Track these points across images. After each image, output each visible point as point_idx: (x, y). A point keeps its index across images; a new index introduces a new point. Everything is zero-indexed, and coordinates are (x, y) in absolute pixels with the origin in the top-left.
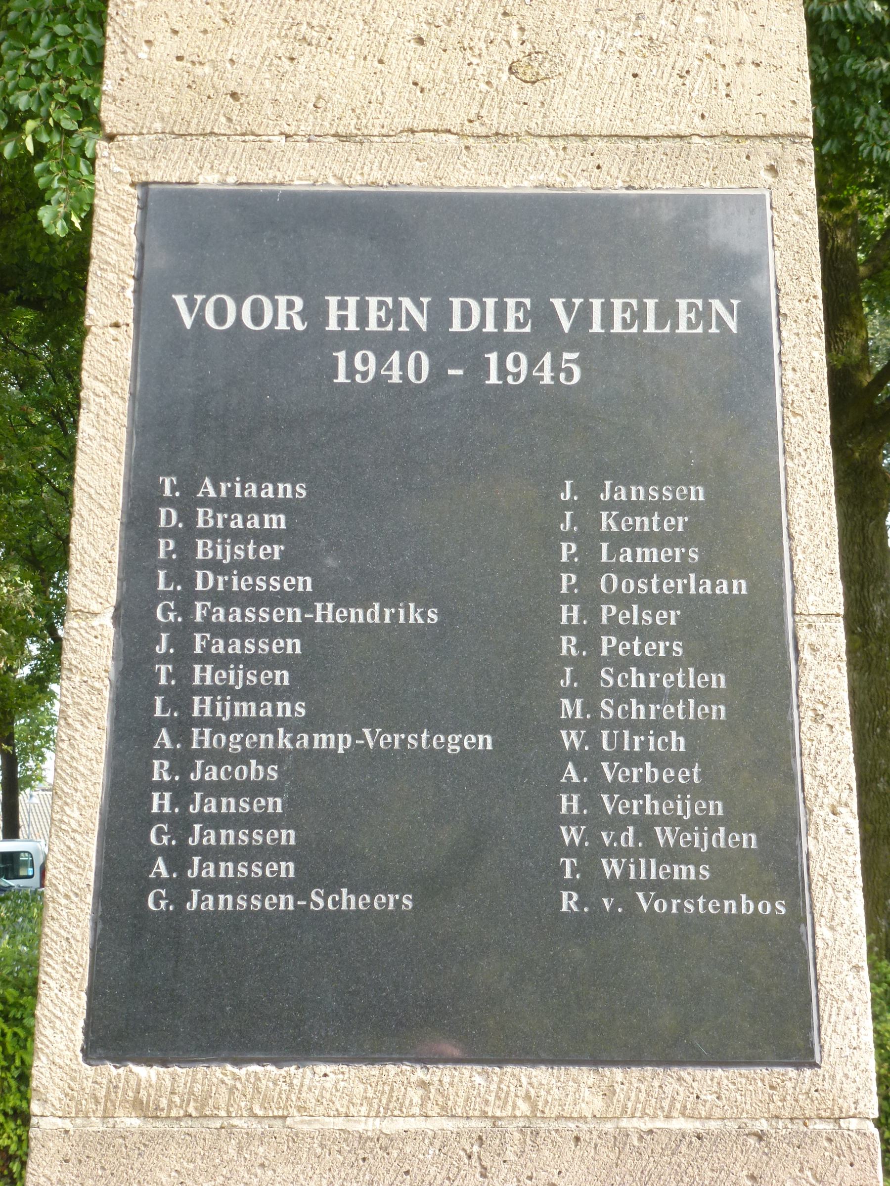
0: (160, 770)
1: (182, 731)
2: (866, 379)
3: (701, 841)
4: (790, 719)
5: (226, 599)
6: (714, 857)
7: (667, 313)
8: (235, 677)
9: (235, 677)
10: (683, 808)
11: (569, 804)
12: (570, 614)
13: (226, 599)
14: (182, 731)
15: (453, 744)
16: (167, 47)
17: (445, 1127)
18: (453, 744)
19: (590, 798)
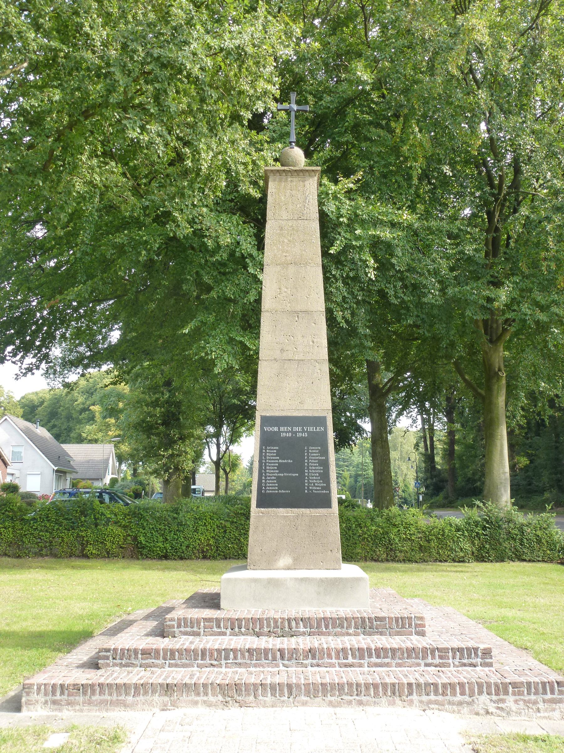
0: (263, 478)
1: (265, 474)
2: (381, 386)
3: (320, 485)
4: (188, 466)
5: (270, 460)
6: (321, 487)
7: (316, 429)
8: (271, 468)
9: (271, 468)
10: (318, 481)
11: (306, 481)
12: (306, 461)
13: (270, 460)
14: (265, 474)
15: (294, 475)
16: (263, 401)
17: (255, 639)
18: (294, 475)
19: (308, 480)
